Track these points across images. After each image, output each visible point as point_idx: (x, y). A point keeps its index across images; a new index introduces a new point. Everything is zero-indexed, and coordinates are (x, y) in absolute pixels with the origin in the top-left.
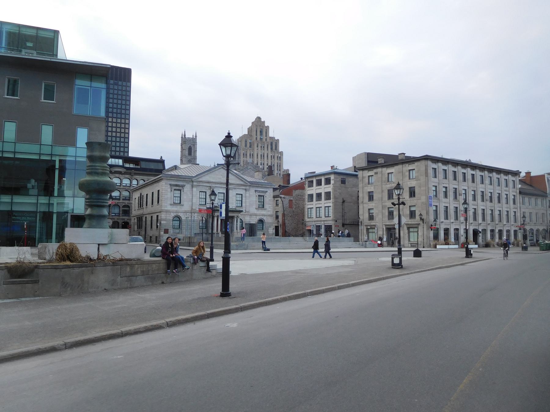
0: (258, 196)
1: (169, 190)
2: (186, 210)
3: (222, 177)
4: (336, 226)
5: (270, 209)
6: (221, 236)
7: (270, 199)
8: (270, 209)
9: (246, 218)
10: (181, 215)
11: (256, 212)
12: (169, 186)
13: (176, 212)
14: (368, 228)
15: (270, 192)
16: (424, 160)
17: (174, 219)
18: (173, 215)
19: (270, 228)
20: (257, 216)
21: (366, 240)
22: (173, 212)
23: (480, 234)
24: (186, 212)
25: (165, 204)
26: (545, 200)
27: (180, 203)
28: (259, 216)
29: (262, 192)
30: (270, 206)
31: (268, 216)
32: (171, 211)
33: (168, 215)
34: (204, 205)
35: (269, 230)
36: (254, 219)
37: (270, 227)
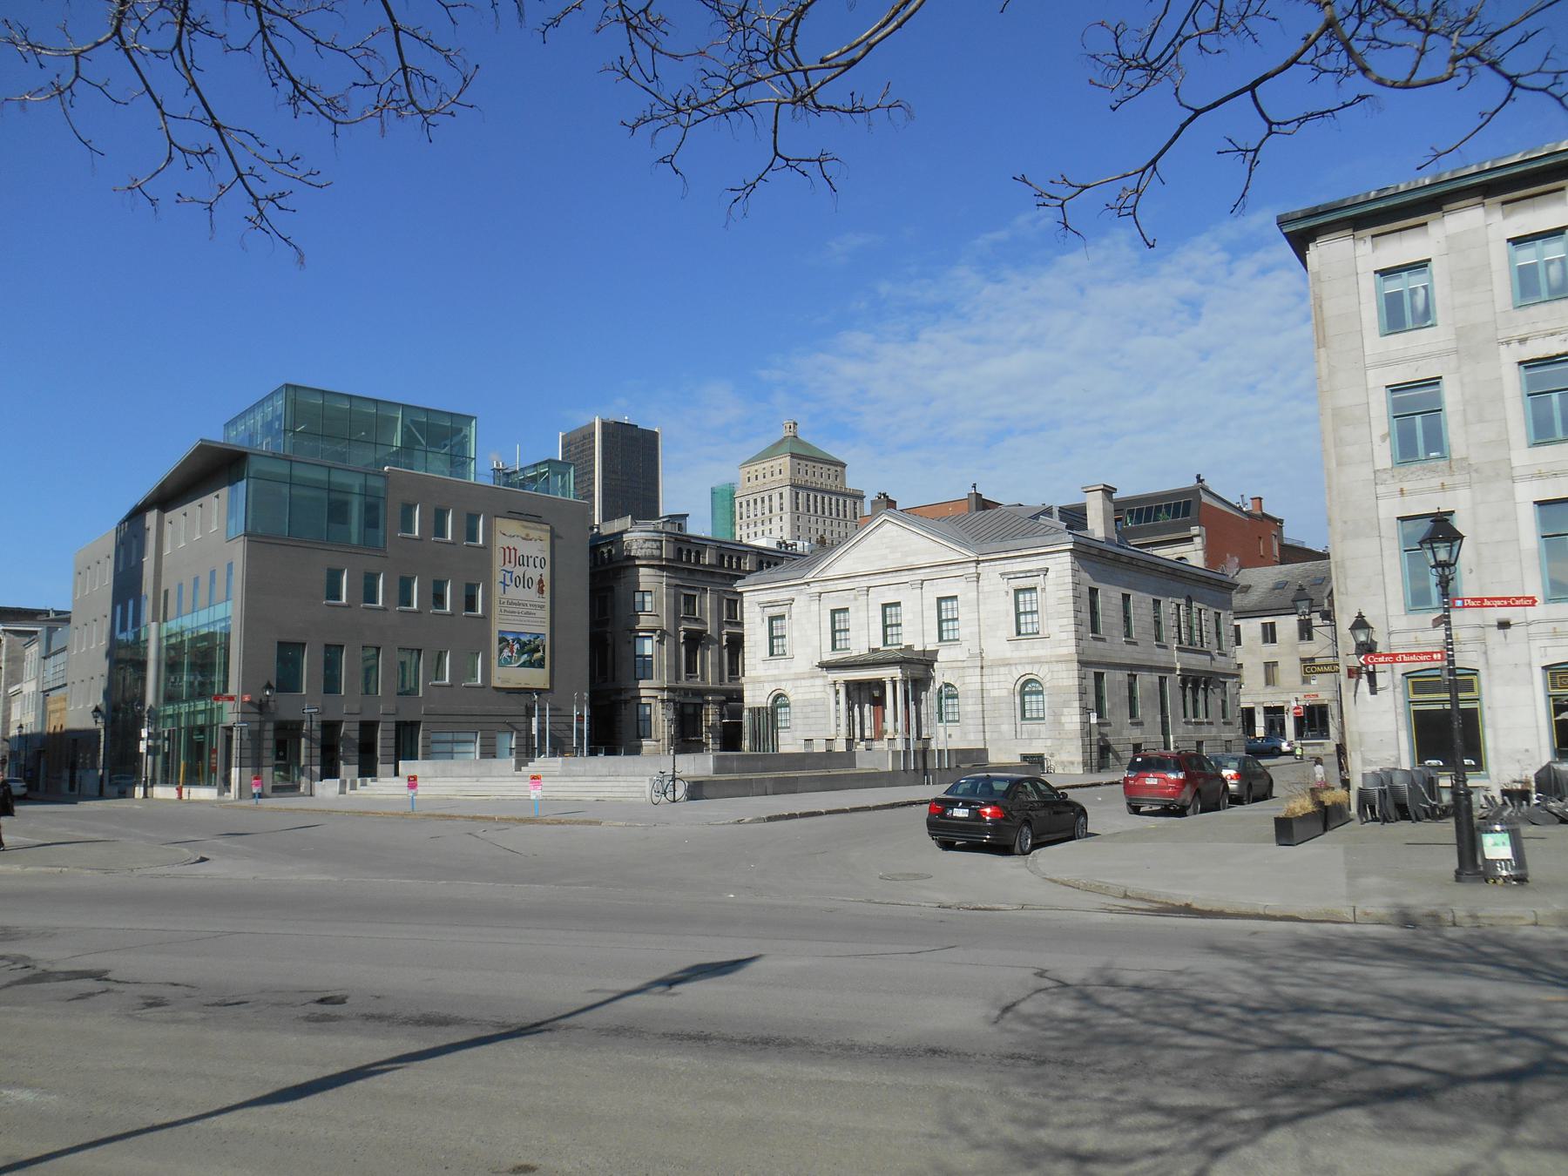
0: (1012, 593)
1: (759, 620)
3: (888, 550)
4: (75, 740)
7: (1062, 594)
9: (967, 680)
10: (787, 688)
11: (1008, 655)
12: (758, 609)
13: (775, 681)
14: (146, 735)
15: (1059, 567)
16: (1349, 232)
18: (769, 688)
19: (1066, 711)
20: (1013, 668)
23: (682, 641)
25: (753, 661)
26: (1054, 985)
28: (1019, 667)
29: (1028, 574)
30: (1065, 621)
31: (1057, 662)
32: (762, 679)
33: (758, 693)
35: (1063, 719)
36: (1002, 678)
37: (1066, 704)
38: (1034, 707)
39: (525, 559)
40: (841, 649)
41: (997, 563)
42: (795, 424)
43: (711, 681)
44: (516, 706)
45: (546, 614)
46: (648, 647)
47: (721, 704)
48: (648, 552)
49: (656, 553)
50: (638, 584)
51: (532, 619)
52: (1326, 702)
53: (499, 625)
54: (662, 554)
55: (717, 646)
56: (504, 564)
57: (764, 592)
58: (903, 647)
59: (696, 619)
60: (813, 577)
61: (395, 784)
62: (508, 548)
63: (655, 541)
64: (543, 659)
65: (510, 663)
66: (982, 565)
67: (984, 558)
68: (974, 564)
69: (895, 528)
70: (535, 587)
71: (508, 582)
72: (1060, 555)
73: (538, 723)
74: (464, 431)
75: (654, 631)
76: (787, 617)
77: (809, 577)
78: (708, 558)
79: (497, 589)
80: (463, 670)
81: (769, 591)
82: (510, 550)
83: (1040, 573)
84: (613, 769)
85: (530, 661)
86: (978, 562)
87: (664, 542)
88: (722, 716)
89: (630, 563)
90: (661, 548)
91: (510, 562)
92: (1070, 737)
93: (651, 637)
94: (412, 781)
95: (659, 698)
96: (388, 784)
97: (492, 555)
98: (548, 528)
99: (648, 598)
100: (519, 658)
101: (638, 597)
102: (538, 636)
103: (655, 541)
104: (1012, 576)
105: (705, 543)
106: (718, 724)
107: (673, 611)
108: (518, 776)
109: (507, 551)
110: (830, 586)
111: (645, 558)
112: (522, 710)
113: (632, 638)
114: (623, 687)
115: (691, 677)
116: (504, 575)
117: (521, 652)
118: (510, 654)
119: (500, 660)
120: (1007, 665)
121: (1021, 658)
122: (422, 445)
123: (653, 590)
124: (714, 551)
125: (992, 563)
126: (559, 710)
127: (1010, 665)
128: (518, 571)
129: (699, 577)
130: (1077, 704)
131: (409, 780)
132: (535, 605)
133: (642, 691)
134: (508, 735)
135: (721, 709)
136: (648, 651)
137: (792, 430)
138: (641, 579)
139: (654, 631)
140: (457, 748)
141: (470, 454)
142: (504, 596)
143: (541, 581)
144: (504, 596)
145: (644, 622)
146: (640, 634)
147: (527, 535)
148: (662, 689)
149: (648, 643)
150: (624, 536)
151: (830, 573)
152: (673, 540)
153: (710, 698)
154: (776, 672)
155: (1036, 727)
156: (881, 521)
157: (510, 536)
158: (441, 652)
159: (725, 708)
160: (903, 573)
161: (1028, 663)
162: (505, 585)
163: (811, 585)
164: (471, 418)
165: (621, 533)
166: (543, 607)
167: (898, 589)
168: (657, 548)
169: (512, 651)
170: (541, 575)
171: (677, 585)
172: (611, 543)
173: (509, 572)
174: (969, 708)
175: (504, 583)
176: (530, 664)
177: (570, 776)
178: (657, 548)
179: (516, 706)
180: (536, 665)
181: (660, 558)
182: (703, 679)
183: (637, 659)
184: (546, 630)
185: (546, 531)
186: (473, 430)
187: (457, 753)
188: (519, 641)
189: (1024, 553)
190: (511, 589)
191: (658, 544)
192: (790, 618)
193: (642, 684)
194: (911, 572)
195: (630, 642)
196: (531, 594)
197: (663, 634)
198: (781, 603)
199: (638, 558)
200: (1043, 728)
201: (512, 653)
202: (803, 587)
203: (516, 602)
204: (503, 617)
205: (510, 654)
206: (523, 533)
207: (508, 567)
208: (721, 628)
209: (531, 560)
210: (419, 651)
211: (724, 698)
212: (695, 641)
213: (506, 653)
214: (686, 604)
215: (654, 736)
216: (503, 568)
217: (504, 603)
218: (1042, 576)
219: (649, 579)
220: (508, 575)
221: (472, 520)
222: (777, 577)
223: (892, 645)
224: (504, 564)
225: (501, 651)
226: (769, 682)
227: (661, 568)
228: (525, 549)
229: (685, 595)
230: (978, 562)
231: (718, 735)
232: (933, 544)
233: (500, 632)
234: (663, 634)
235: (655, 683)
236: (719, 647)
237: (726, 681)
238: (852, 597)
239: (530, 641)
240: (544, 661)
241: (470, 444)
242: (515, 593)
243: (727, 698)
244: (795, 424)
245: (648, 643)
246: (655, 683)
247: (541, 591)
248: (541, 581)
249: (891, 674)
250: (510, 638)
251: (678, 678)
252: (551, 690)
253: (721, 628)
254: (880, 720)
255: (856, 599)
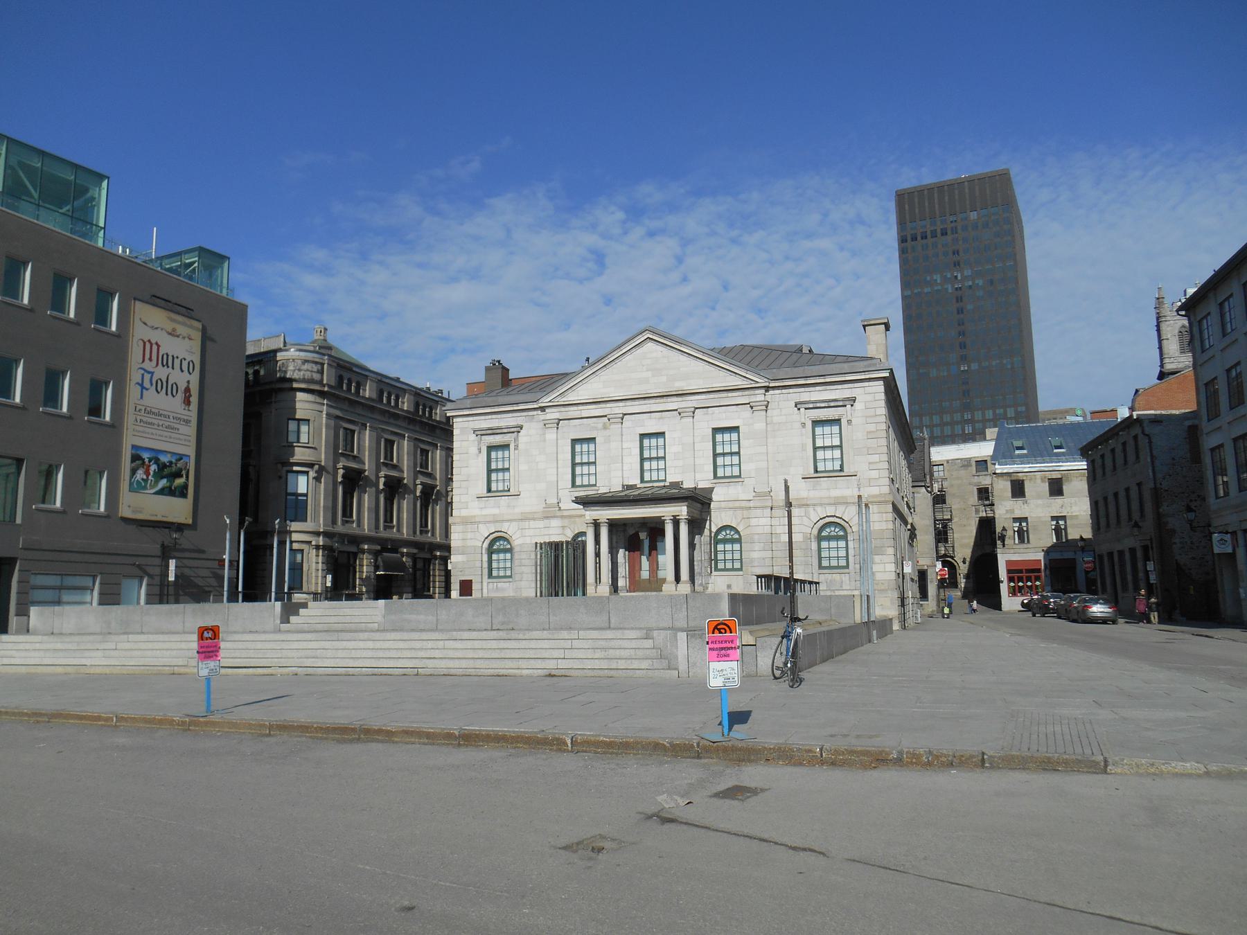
0: (809, 425)
1: (474, 450)
2: (528, 509)
3: (649, 374)
5: (874, 474)
6: (716, 597)
7: (872, 427)
8: (874, 474)
9: (754, 522)
10: (510, 530)
15: (869, 398)
17: (824, 534)
18: (485, 530)
19: (877, 558)
20: (811, 509)
21: (933, 611)
22: (821, 505)
24: (525, 518)
27: (842, 470)
28: (819, 509)
30: (876, 458)
32: (477, 520)
33: (469, 535)
34: (837, 471)
35: (876, 568)
38: (729, 556)
39: (170, 358)
40: (582, 486)
41: (791, 390)
42: (326, 329)
43: (366, 528)
44: (150, 544)
45: (190, 431)
46: (302, 484)
47: (376, 554)
48: (308, 375)
49: (316, 376)
50: (294, 410)
51: (173, 435)
52: (926, 568)
53: (131, 438)
54: (322, 379)
55: (374, 489)
56: (143, 361)
57: (483, 417)
58: (667, 484)
59: (355, 457)
60: (550, 401)
61: (38, 646)
62: (149, 341)
63: (316, 363)
64: (185, 486)
65: (145, 488)
66: (771, 392)
67: (777, 384)
68: (763, 391)
69: (660, 348)
70: (180, 396)
71: (147, 384)
72: (871, 384)
73: (176, 567)
74: (91, 191)
75: (311, 465)
76: (512, 447)
77: (545, 401)
78: (368, 391)
79: (133, 392)
80: (81, 486)
81: (490, 417)
82: (145, 343)
83: (847, 403)
84: (500, 618)
85: (170, 488)
86: (767, 389)
87: (326, 366)
88: (377, 568)
89: (287, 385)
90: (322, 372)
91: (150, 359)
92: (883, 588)
93: (307, 473)
94: (209, 642)
95: (313, 543)
96: (21, 647)
97: (127, 346)
98: (199, 325)
99: (304, 428)
100: (156, 482)
101: (292, 426)
102: (181, 457)
103: (316, 363)
104: (811, 406)
105: (367, 373)
106: (372, 576)
107: (332, 445)
108: (288, 631)
109: (148, 346)
110: (573, 412)
111: (304, 381)
112: (156, 549)
113: (284, 475)
114: (269, 529)
115: (347, 522)
116: (143, 375)
117: (159, 475)
118: (145, 477)
119: (131, 484)
120: (803, 505)
121: (821, 498)
122: (32, 197)
123: (312, 419)
124: (375, 385)
125: (784, 391)
126: (203, 552)
127: (807, 505)
128: (161, 373)
129: (359, 410)
130: (891, 551)
131: (201, 637)
132: (180, 419)
133: (293, 535)
134: (136, 582)
135: (376, 560)
136: (302, 489)
137: (322, 334)
138: (298, 405)
139: (311, 465)
140: (66, 597)
141: (93, 221)
142: (141, 402)
143: (187, 390)
144: (141, 402)
145: (300, 454)
146: (295, 468)
147: (174, 330)
148: (317, 534)
149: (302, 480)
150: (278, 354)
151: (572, 397)
152: (335, 364)
153: (366, 547)
154: (496, 511)
155: (837, 577)
156: (643, 339)
157: (153, 328)
158: (51, 466)
159: (379, 559)
160: (670, 399)
161: (830, 504)
162: (143, 387)
163: (547, 410)
164: (101, 177)
165: (275, 352)
166: (187, 422)
167: (661, 418)
168: (318, 372)
169: (147, 473)
170: (188, 382)
171: (337, 417)
172: (260, 362)
173: (149, 372)
174: (755, 555)
175: (141, 385)
176: (169, 491)
177: (402, 630)
178: (318, 372)
179: (150, 544)
180: (177, 493)
181: (320, 382)
182: (359, 525)
183: (288, 497)
184: (190, 451)
185: (197, 329)
186: (104, 193)
187: (157, 595)
188: (157, 461)
189: (828, 380)
190: (150, 394)
191: (319, 367)
192: (516, 448)
193: (294, 526)
194: (680, 399)
195: (280, 477)
196: (174, 404)
197: (321, 470)
198: (505, 431)
199: (295, 380)
200: (845, 578)
201: (148, 476)
202: (535, 413)
203: (157, 411)
204: (137, 428)
205: (145, 477)
206: (169, 328)
207: (148, 365)
208: (378, 470)
209: (177, 362)
210: (19, 462)
211: (379, 548)
212: (354, 481)
213: (140, 474)
214: (343, 444)
215: (305, 589)
216: (142, 366)
217: (140, 410)
218: (849, 406)
219: (307, 406)
220: (147, 377)
221: (104, 297)
222: (501, 400)
223: (651, 481)
224: (143, 361)
225: (134, 472)
226: (485, 523)
227: (321, 394)
228: (170, 346)
229: (345, 428)
230: (767, 389)
231: (372, 588)
232: (708, 367)
233: (134, 447)
234: (321, 470)
235: (309, 525)
236: (376, 490)
237: (382, 528)
238: (600, 426)
239: (171, 463)
240: (187, 489)
241: (99, 208)
242: (154, 399)
243: (382, 548)
244: (326, 329)
245: (302, 480)
246: (309, 525)
247: (187, 402)
248: (187, 390)
249: (673, 512)
250: (146, 456)
251: (334, 522)
252: (193, 527)
253: (378, 470)
254: (637, 568)
255: (605, 428)
